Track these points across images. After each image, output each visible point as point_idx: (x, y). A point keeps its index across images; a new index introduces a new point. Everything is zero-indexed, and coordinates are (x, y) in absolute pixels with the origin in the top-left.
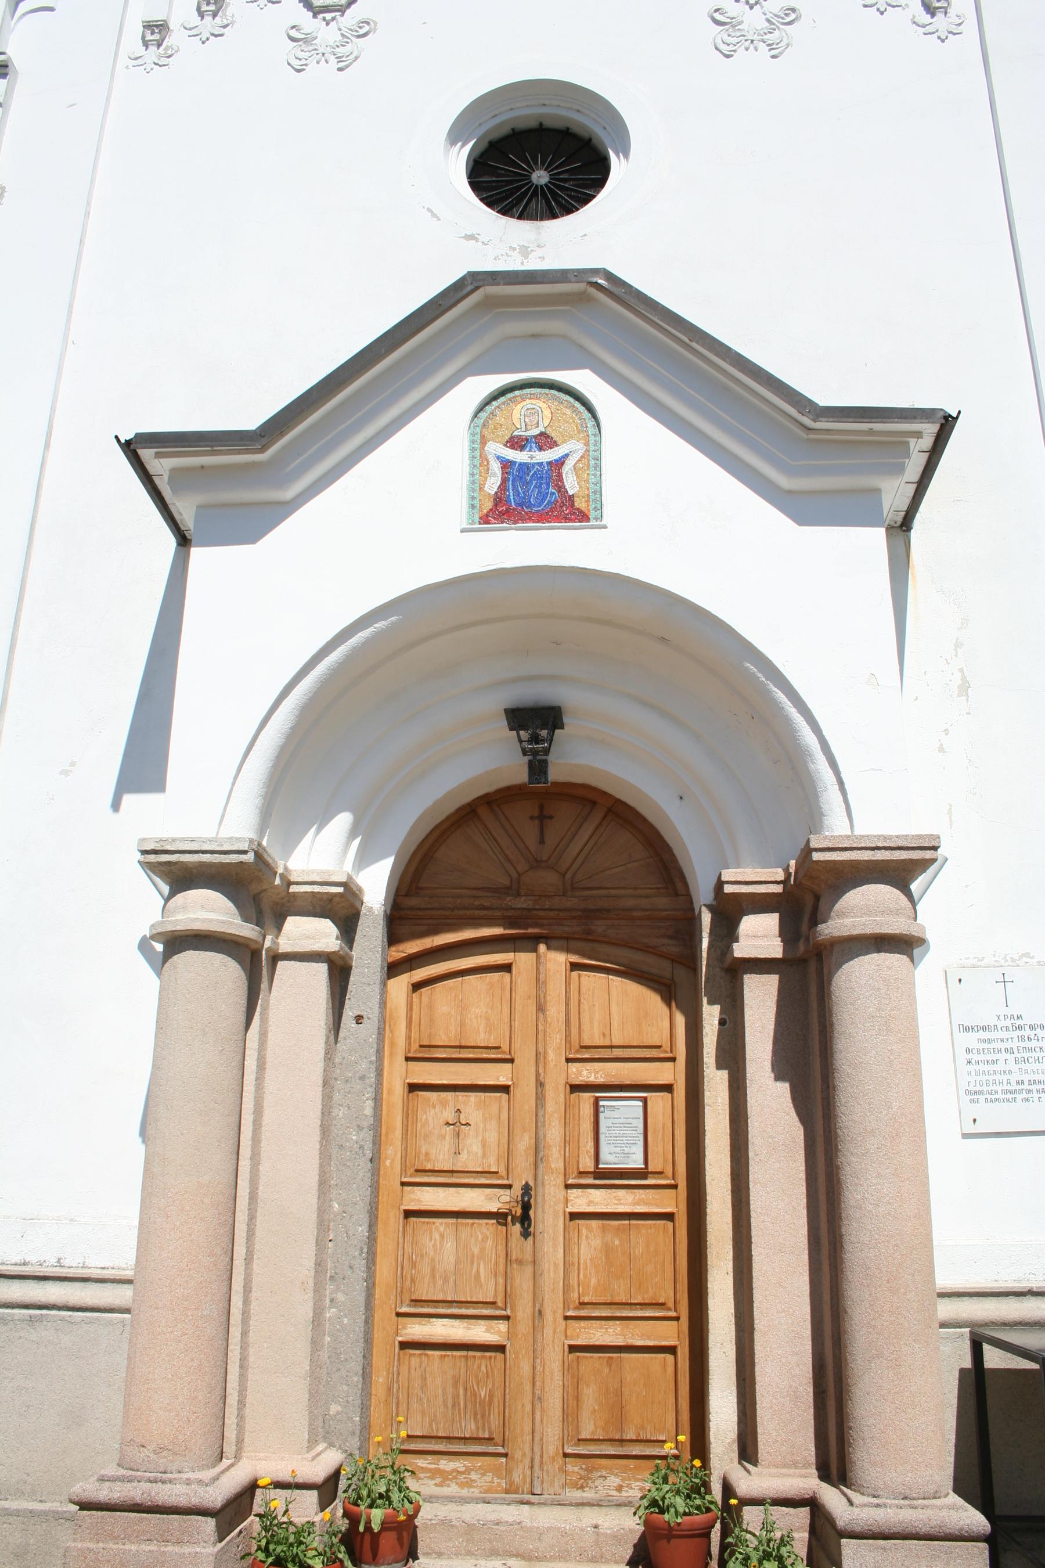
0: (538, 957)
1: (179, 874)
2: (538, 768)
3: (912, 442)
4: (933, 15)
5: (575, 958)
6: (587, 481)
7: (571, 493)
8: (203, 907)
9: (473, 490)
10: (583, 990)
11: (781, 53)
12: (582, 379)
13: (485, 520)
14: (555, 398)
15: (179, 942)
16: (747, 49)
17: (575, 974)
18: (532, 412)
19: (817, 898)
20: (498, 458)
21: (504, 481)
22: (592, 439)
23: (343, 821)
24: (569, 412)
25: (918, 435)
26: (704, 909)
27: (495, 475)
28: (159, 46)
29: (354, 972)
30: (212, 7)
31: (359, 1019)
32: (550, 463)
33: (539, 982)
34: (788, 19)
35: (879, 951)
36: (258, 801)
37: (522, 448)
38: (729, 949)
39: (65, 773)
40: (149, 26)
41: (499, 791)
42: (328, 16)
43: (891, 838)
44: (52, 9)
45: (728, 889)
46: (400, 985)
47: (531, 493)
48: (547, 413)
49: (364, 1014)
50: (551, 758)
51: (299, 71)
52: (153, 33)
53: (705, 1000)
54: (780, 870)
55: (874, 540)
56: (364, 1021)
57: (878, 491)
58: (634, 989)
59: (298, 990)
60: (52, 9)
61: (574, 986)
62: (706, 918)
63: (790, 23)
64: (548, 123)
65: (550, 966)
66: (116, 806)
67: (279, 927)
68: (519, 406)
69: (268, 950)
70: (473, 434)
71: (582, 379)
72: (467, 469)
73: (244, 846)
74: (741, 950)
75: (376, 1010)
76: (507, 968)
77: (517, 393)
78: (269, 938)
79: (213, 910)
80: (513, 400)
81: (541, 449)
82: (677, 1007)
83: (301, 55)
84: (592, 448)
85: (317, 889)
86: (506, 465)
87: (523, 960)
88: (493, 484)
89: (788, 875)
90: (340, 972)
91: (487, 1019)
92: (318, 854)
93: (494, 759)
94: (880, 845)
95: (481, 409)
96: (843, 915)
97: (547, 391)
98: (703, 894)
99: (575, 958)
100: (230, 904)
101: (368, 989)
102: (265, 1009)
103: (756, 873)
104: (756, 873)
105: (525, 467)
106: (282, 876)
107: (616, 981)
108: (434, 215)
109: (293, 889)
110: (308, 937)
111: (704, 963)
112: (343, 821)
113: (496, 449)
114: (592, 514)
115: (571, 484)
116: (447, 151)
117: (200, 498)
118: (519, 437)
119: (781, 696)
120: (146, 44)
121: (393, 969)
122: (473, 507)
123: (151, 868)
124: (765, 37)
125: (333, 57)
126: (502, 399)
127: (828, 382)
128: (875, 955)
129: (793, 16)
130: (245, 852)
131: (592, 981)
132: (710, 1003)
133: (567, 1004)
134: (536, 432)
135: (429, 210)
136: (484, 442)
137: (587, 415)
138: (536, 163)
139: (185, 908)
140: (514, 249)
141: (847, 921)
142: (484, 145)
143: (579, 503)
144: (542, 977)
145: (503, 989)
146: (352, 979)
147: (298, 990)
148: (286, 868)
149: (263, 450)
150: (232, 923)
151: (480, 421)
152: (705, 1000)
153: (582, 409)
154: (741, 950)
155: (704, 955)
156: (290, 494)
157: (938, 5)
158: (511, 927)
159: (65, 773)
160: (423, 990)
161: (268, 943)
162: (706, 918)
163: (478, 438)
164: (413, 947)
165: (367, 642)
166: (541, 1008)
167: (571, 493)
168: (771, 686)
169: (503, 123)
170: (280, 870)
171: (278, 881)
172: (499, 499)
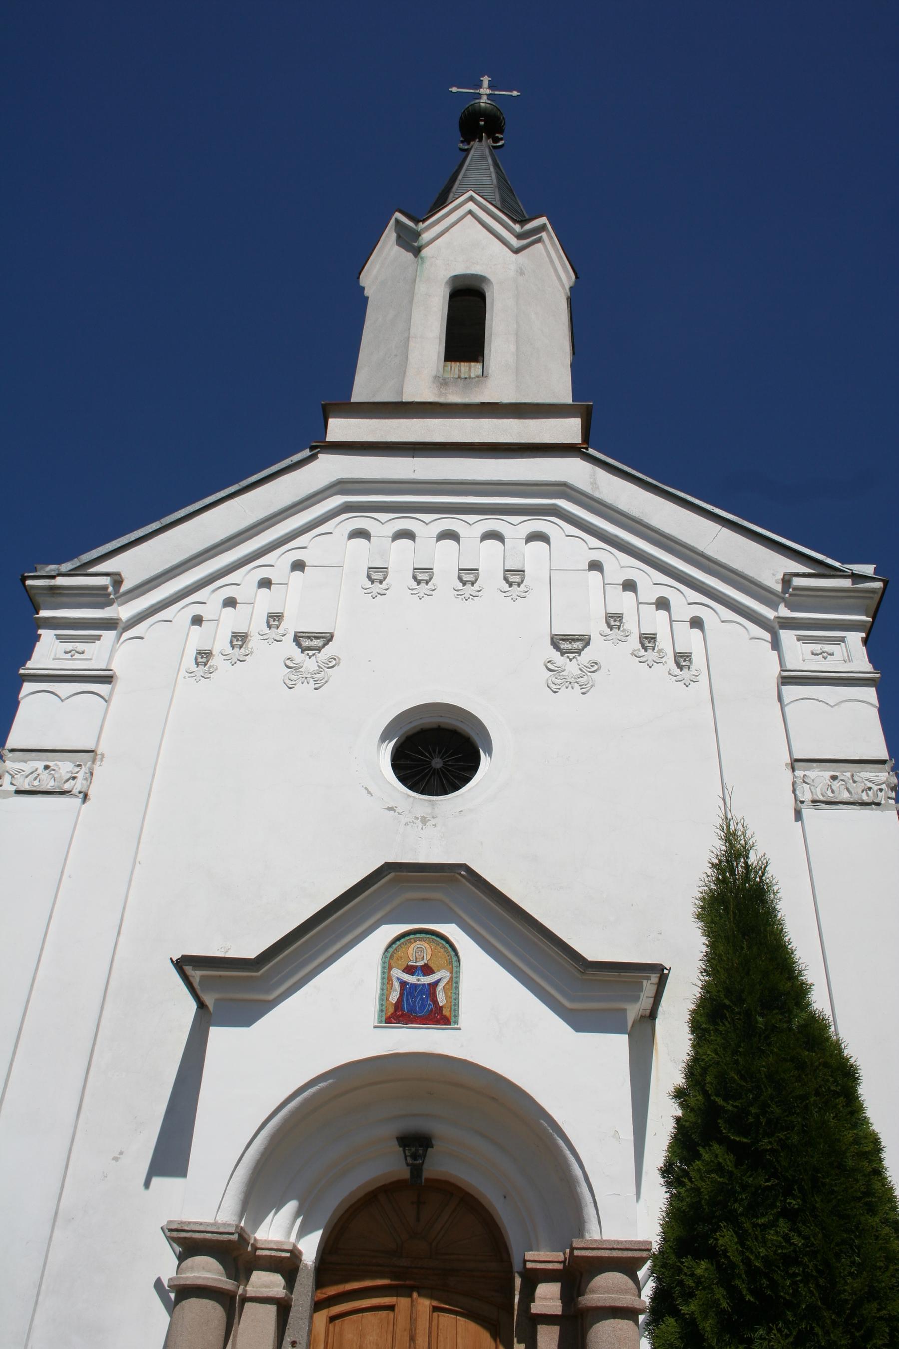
0: (412, 1301)
1: (189, 1243)
2: (416, 1170)
3: (645, 982)
4: (681, 669)
5: (435, 1303)
6: (451, 998)
7: (441, 1004)
8: (203, 1268)
9: (382, 1000)
10: (440, 1327)
11: (588, 691)
12: (450, 930)
13: (388, 1020)
14: (433, 941)
15: (186, 1292)
16: (567, 688)
17: (435, 1314)
18: (420, 950)
19: (582, 1274)
20: (398, 979)
21: (401, 994)
22: (455, 969)
23: (291, 1206)
24: (442, 950)
25: (649, 978)
26: (517, 1275)
27: (396, 990)
28: (205, 664)
29: (293, 1309)
30: (239, 643)
31: (294, 1343)
32: (429, 984)
33: (412, 1319)
34: (593, 669)
35: (614, 1318)
36: (241, 1196)
37: (412, 974)
38: (529, 1308)
39: (116, 1159)
40: (200, 653)
41: (391, 1183)
42: (311, 653)
43: (621, 1242)
44: (142, 638)
45: (530, 1265)
46: (321, 1317)
47: (417, 1005)
48: (429, 951)
49: (297, 1340)
50: (425, 1166)
51: (290, 688)
52: (202, 657)
53: (516, 1340)
54: (561, 1253)
55: (618, 1045)
56: (298, 1345)
57: (625, 1010)
58: (473, 1326)
59: (257, 1322)
60: (142, 638)
61: (434, 1323)
62: (518, 1281)
63: (594, 672)
64: (442, 726)
65: (419, 1307)
66: (147, 1184)
67: (248, 1278)
68: (412, 946)
69: (240, 1295)
70: (384, 963)
71: (450, 930)
72: (379, 986)
73: (232, 1230)
74: (537, 1307)
75: (305, 1337)
76: (391, 1308)
77: (412, 936)
78: (242, 1287)
79: (209, 1271)
80: (410, 942)
81: (424, 975)
82: (501, 1341)
83: (293, 677)
84: (455, 975)
85: (273, 1253)
86: (403, 984)
87: (402, 1302)
88: (394, 997)
89: (566, 1258)
90: (283, 1308)
91: (377, 1345)
92: (276, 1229)
93: (390, 1164)
94: (615, 1246)
95: (390, 945)
96: (593, 1291)
97: (429, 936)
98: (517, 1266)
99: (435, 1303)
100: (221, 1267)
101: (301, 1322)
102: (235, 1337)
103: (544, 1256)
104: (544, 1256)
105: (414, 986)
106: (253, 1245)
107: (462, 1320)
108: (369, 793)
109: (259, 1252)
110: (266, 1286)
111: (516, 1313)
112: (291, 1206)
113: (397, 973)
114: (453, 1020)
115: (441, 999)
116: (379, 747)
117: (217, 996)
118: (412, 966)
119: (561, 1142)
120: (197, 663)
121: (318, 1306)
122: (381, 1011)
123: (172, 1239)
124: (578, 680)
125: (312, 680)
126: (402, 940)
127: (594, 947)
128: (612, 1320)
129: (596, 667)
130: (232, 1234)
131: (446, 1320)
132: (519, 1342)
133: (429, 1336)
134: (421, 963)
135: (366, 789)
136: (390, 968)
137: (453, 953)
138: (434, 752)
139: (192, 1268)
140: (417, 819)
141: (595, 1296)
142: (403, 738)
143: (446, 1012)
144: (414, 1315)
145: (388, 1323)
146: (291, 1314)
147: (257, 1322)
148: (255, 1239)
149: (257, 971)
150: (221, 1280)
151: (388, 955)
152: (516, 1340)
153: (450, 949)
154: (537, 1307)
155: (516, 1307)
156: (271, 997)
157: (684, 663)
158: (394, 1280)
159: (116, 1159)
160: (337, 1321)
161: (240, 1291)
162: (518, 1281)
163: (386, 965)
164: (332, 1291)
165: (314, 1095)
166: (412, 1338)
167: (441, 1004)
168: (556, 1136)
169: (414, 727)
170: (252, 1241)
171: (249, 1248)
172: (398, 1005)
